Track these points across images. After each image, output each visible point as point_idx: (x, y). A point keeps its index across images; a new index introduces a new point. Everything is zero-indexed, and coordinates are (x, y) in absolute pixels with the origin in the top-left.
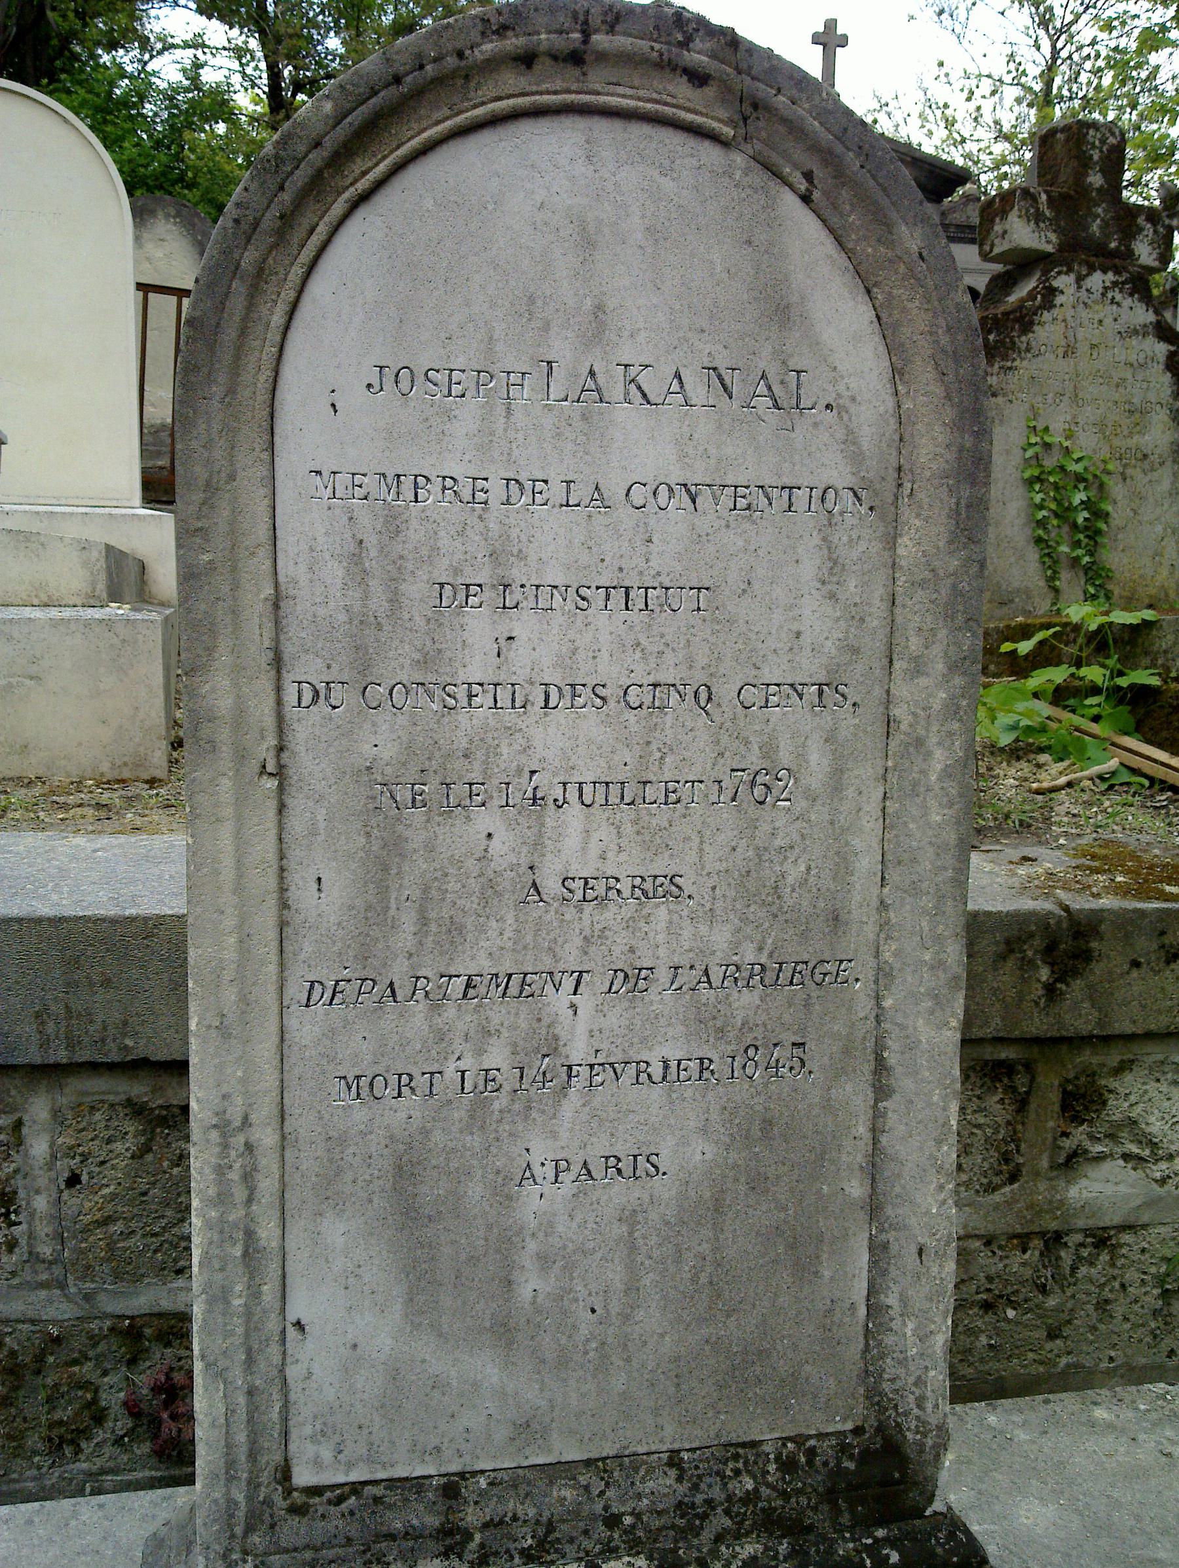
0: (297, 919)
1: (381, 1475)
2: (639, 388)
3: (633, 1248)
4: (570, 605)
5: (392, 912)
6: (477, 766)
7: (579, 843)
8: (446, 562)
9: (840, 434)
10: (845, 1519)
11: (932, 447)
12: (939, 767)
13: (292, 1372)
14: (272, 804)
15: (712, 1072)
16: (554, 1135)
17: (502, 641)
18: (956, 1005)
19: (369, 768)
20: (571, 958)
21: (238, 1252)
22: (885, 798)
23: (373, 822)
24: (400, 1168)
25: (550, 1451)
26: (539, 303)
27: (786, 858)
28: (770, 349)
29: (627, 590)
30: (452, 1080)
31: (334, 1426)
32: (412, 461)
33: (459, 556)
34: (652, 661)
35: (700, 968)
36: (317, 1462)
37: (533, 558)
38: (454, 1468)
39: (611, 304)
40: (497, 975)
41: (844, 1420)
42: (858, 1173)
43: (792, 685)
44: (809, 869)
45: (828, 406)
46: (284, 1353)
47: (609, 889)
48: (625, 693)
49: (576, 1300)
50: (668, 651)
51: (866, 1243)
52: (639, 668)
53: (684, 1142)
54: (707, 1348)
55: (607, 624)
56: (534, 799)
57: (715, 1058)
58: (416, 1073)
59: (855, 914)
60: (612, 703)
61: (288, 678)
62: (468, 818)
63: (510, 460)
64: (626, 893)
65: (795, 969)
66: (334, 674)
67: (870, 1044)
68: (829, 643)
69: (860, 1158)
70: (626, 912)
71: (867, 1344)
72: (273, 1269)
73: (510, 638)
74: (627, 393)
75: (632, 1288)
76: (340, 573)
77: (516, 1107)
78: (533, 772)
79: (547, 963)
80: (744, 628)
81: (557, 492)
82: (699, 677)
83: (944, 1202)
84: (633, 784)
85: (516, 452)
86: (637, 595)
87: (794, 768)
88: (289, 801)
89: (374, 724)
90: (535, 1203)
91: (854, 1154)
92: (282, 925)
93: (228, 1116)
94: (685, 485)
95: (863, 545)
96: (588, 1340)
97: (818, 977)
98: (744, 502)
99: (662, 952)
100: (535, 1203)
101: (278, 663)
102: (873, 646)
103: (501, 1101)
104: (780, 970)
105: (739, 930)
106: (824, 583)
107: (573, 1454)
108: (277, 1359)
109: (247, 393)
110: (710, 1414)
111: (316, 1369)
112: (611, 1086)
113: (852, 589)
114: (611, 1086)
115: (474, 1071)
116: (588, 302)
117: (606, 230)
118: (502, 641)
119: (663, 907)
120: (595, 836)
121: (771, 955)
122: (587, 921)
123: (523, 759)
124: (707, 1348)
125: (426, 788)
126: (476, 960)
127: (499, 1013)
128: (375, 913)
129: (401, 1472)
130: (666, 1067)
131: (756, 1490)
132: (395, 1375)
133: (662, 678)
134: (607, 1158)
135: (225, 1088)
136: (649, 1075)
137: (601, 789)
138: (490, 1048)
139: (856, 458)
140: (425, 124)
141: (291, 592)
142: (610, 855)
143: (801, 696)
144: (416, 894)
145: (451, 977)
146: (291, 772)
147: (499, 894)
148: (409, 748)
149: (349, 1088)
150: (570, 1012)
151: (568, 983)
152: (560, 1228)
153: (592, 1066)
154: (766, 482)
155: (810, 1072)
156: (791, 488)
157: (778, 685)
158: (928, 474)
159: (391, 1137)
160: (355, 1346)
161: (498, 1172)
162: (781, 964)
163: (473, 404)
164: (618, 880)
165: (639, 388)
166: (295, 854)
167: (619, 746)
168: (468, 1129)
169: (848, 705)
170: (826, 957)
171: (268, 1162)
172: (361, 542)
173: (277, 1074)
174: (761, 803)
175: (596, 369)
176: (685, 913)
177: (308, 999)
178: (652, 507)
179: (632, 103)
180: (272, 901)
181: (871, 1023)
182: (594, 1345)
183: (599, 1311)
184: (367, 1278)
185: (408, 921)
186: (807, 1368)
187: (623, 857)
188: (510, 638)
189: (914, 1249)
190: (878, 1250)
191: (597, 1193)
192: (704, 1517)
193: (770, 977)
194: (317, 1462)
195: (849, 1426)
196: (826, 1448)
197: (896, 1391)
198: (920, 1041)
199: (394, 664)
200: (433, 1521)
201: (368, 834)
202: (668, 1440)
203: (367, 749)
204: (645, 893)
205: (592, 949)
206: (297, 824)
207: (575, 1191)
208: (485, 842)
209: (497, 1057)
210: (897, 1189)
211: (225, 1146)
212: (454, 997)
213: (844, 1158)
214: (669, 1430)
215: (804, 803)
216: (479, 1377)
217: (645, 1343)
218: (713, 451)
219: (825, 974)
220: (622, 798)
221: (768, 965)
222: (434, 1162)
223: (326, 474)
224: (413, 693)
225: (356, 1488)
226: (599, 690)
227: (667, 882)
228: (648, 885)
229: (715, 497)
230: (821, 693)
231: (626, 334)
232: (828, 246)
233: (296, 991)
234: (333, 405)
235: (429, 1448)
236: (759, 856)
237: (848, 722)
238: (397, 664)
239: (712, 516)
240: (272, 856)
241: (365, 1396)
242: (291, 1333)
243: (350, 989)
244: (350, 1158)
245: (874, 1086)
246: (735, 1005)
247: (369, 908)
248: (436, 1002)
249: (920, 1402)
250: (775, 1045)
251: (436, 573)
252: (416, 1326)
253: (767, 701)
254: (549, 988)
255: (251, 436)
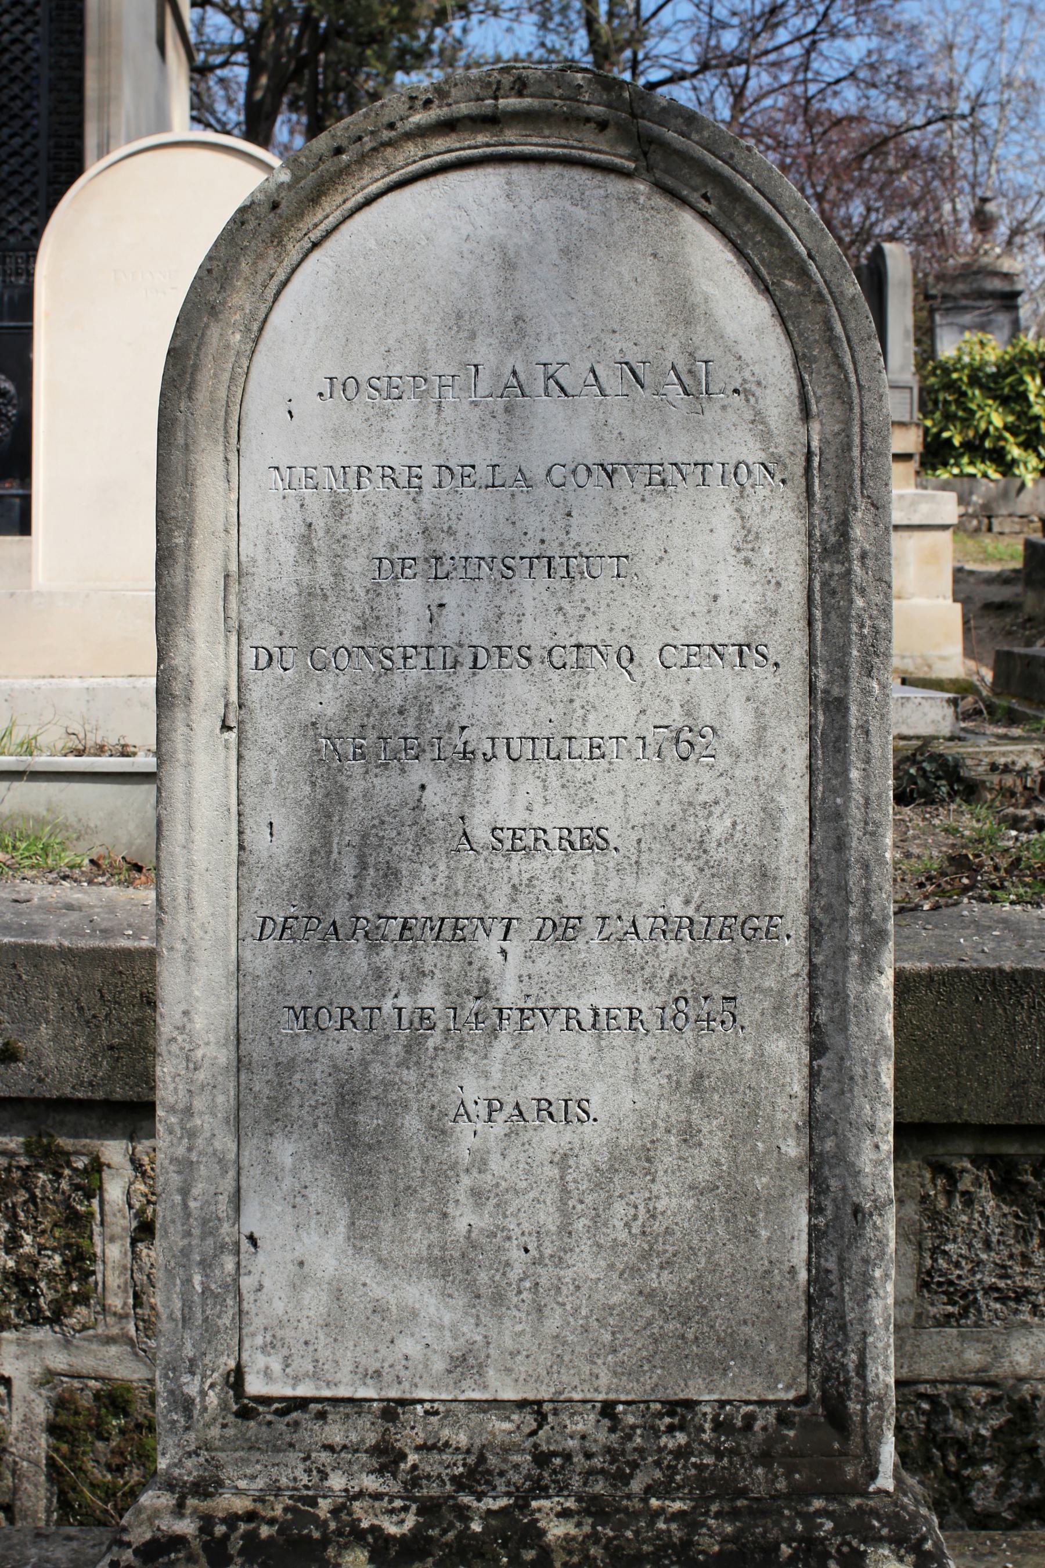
0: (252, 859)
1: (327, 1393)
3: (565, 1190)
5: (335, 856)
6: (411, 721)
8: (384, 539)
9: (749, 415)
13: (247, 1283)
17: (434, 609)
19: (314, 724)
20: (500, 905)
23: (317, 773)
24: (342, 1096)
25: (485, 1387)
26: (467, 317)
27: (710, 814)
30: (390, 1017)
32: (357, 455)
33: (395, 533)
35: (627, 917)
36: (267, 1373)
37: (461, 535)
38: (393, 1394)
39: (528, 314)
41: (788, 1388)
44: (734, 824)
45: (736, 391)
46: (238, 1263)
47: (536, 839)
50: (589, 615)
52: (563, 631)
58: (357, 1008)
60: (536, 664)
61: (246, 644)
62: (403, 771)
64: (554, 843)
66: (286, 640)
69: (795, 1116)
70: (555, 862)
74: (546, 388)
75: (565, 1229)
76: (293, 551)
77: (449, 1045)
78: (463, 728)
79: (477, 909)
80: (662, 593)
84: (558, 738)
85: (446, 442)
86: (559, 563)
87: (717, 726)
88: (245, 753)
89: (319, 684)
90: (469, 1140)
95: (775, 515)
96: (521, 1280)
99: (589, 902)
100: (469, 1140)
103: (434, 1040)
105: (665, 883)
106: (738, 550)
107: (509, 1394)
111: (267, 1283)
114: (541, 1033)
116: (510, 313)
117: (524, 254)
118: (434, 609)
120: (522, 789)
121: (698, 909)
127: (432, 956)
129: (343, 1392)
130: (596, 1014)
131: (688, 1445)
139: (766, 437)
140: (364, 182)
141: (251, 570)
142: (535, 807)
144: (356, 840)
147: (431, 842)
148: (350, 707)
151: (498, 930)
152: (493, 1166)
153: (522, 1010)
154: (679, 459)
159: (335, 1066)
163: (409, 403)
166: (249, 800)
167: (543, 704)
168: (403, 1064)
170: (755, 911)
176: (611, 865)
179: (542, 150)
181: (803, 981)
184: (313, 1198)
185: (349, 864)
186: (747, 1329)
187: (550, 809)
191: (528, 1135)
192: (634, 1465)
194: (267, 1373)
195: (791, 1395)
196: (767, 1418)
199: (338, 630)
200: (372, 1438)
201: (313, 784)
202: (604, 1390)
203: (314, 707)
204: (571, 844)
205: (521, 897)
206: (252, 775)
208: (418, 793)
209: (431, 996)
213: (779, 1116)
214: (604, 1380)
217: (578, 1288)
218: (626, 433)
221: (696, 919)
222: (374, 1093)
225: (301, 1403)
228: (576, 837)
230: (741, 653)
231: (544, 338)
232: (730, 256)
236: (684, 811)
237: (765, 680)
241: (311, 1313)
244: (298, 1084)
246: (662, 957)
247: (314, 851)
248: (374, 941)
251: (374, 550)
252: (358, 1250)
254: (480, 933)
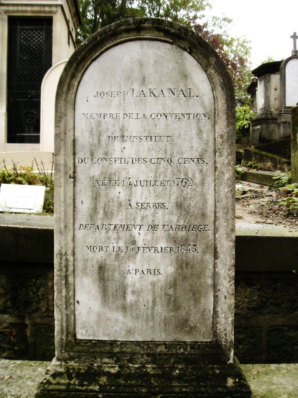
1: (96, 339)
2: (153, 94)
4: (138, 140)
7: (140, 195)
9: (200, 102)
10: (206, 362)
11: (222, 104)
12: (227, 178)
14: (72, 184)
15: (173, 251)
16: (135, 264)
17: (122, 149)
18: (233, 236)
19: (93, 177)
21: (64, 282)
22: (215, 186)
28: (183, 85)
29: (151, 137)
31: (86, 326)
34: (157, 153)
35: (170, 225)
40: (121, 225)
41: (208, 339)
42: (210, 278)
43: (191, 159)
44: (196, 202)
45: (197, 96)
47: (147, 206)
48: (151, 160)
49: (141, 303)
51: (213, 295)
53: (166, 267)
54: (173, 318)
55: (146, 144)
56: (130, 184)
57: (174, 248)
58: (103, 247)
59: (208, 214)
60: (148, 163)
62: (115, 188)
63: (124, 110)
64: (152, 207)
65: (193, 227)
67: (213, 246)
68: (200, 149)
71: (213, 320)
72: (72, 287)
73: (124, 148)
74: (150, 95)
75: (154, 302)
78: (129, 178)
79: (133, 223)
81: (135, 116)
82: (168, 157)
83: (231, 285)
86: (153, 138)
87: (192, 178)
91: (209, 273)
92: (74, 211)
93: (62, 252)
94: (164, 114)
95: (207, 127)
97: (200, 229)
98: (178, 117)
101: (74, 154)
102: (211, 149)
103: (123, 254)
104: (190, 227)
107: (140, 339)
108: (73, 309)
109: (69, 99)
110: (174, 334)
112: (148, 253)
113: (205, 137)
115: (116, 247)
119: (160, 211)
120: (144, 193)
122: (142, 214)
123: (127, 175)
124: (173, 318)
125: (105, 182)
126: (116, 221)
128: (95, 210)
129: (100, 339)
132: (99, 316)
133: (159, 157)
134: (148, 270)
135: (61, 246)
136: (158, 251)
137: (145, 182)
138: (120, 242)
139: (204, 107)
143: (193, 161)
145: (111, 225)
146: (77, 177)
148: (102, 173)
149: (89, 249)
150: (139, 234)
151: (138, 228)
154: (183, 113)
155: (198, 252)
156: (189, 114)
157: (188, 159)
158: (221, 110)
159: (98, 261)
160: (90, 308)
161: (122, 271)
162: (190, 225)
163: (117, 98)
164: (149, 204)
165: (153, 94)
168: (115, 261)
169: (205, 164)
171: (71, 264)
172: (92, 128)
173: (73, 244)
174: (184, 186)
175: (143, 90)
177: (80, 228)
178: (156, 119)
179: (150, 37)
180: (72, 205)
181: (213, 241)
182: (145, 314)
183: (146, 306)
188: (124, 148)
189: (224, 297)
190: (216, 297)
193: (187, 228)
194: (82, 334)
197: (220, 332)
198: (224, 245)
206: (78, 189)
207: (140, 277)
208: (118, 194)
210: (220, 282)
211: (61, 259)
212: (112, 230)
213: (207, 274)
215: (195, 187)
216: (118, 318)
218: (170, 106)
219: (201, 228)
220: (150, 185)
223: (85, 115)
224: (103, 160)
226: (145, 159)
227: (161, 205)
228: (157, 205)
229: (171, 116)
230: (198, 160)
233: (77, 226)
234: (87, 101)
235: (107, 334)
238: (100, 154)
239: (170, 120)
240: (72, 195)
242: (76, 303)
243: (89, 226)
245: (214, 256)
249: (226, 335)
250: (189, 245)
253: (185, 162)
254: (133, 229)
255: (70, 107)
